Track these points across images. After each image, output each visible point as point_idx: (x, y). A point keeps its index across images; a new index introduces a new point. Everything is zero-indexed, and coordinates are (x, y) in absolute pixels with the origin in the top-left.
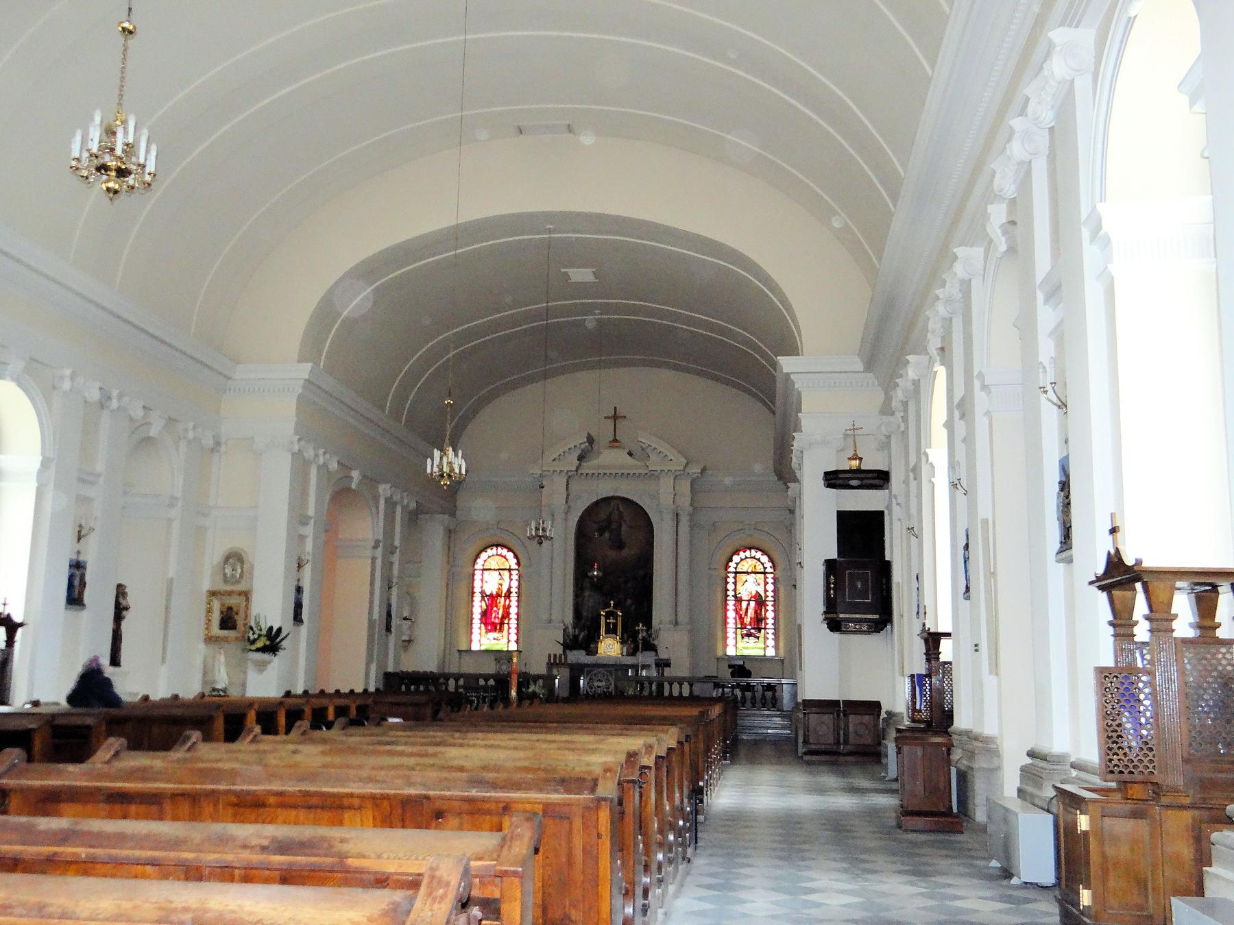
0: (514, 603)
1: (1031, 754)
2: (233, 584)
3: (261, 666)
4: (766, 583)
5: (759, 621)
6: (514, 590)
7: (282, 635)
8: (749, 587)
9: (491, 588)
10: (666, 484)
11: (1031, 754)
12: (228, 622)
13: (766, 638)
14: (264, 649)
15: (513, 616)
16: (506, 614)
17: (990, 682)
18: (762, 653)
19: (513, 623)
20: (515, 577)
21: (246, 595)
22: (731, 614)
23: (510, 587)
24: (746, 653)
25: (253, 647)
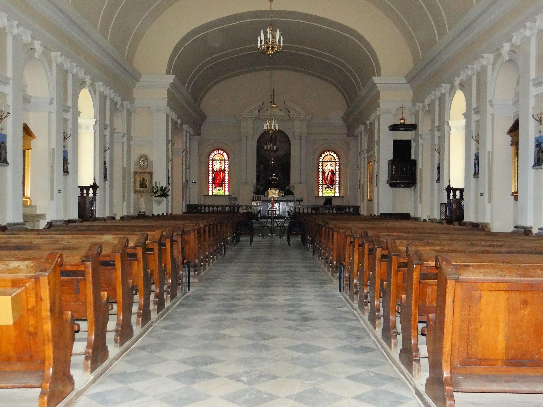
0: (227, 175)
1: (515, 227)
2: (144, 169)
3: (159, 203)
4: (336, 166)
5: (333, 181)
6: (227, 169)
7: (167, 190)
8: (329, 167)
9: (217, 167)
10: (297, 123)
11: (515, 227)
12: (143, 185)
13: (335, 189)
14: (161, 196)
15: (227, 180)
16: (224, 179)
17: (488, 206)
18: (333, 195)
19: (227, 182)
20: (227, 163)
21: (151, 174)
22: (321, 179)
23: (225, 168)
24: (327, 195)
25: (157, 195)
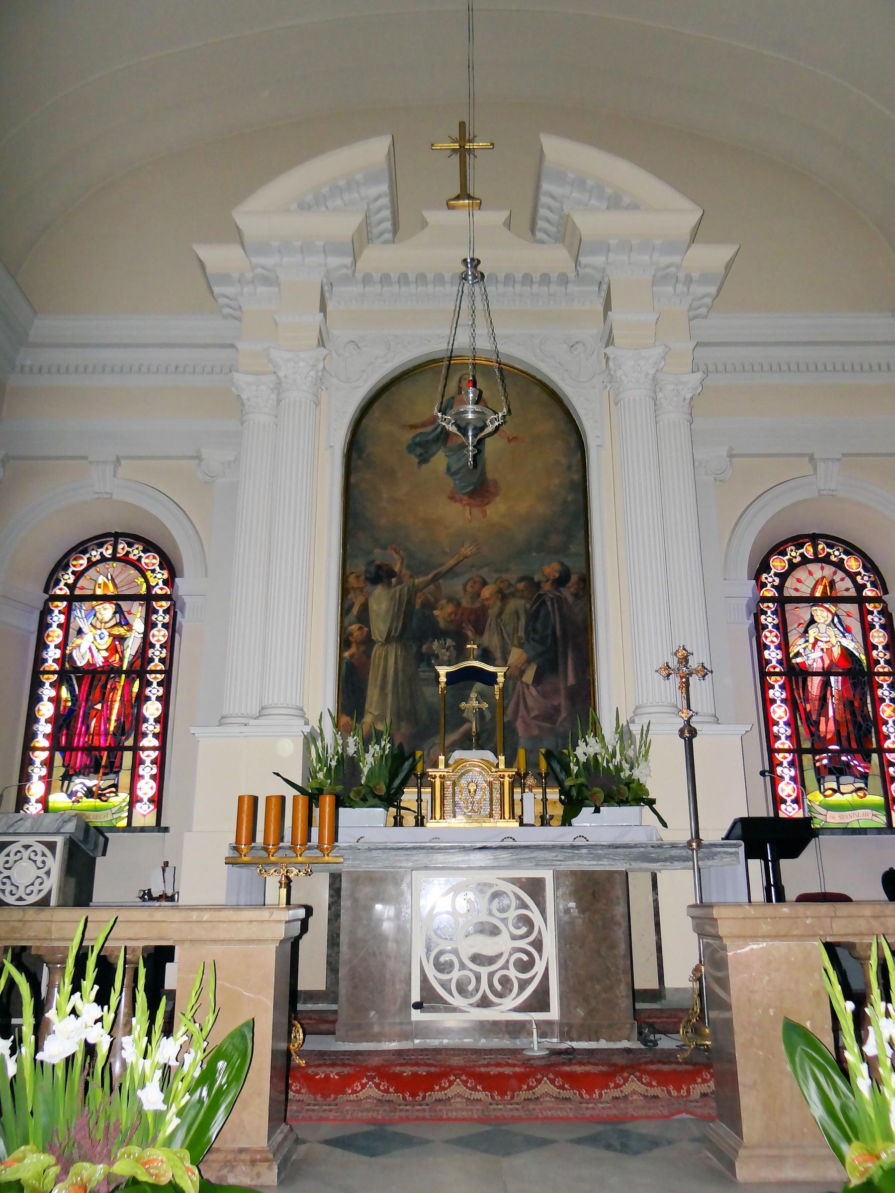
4: (867, 628)
9: (90, 648)
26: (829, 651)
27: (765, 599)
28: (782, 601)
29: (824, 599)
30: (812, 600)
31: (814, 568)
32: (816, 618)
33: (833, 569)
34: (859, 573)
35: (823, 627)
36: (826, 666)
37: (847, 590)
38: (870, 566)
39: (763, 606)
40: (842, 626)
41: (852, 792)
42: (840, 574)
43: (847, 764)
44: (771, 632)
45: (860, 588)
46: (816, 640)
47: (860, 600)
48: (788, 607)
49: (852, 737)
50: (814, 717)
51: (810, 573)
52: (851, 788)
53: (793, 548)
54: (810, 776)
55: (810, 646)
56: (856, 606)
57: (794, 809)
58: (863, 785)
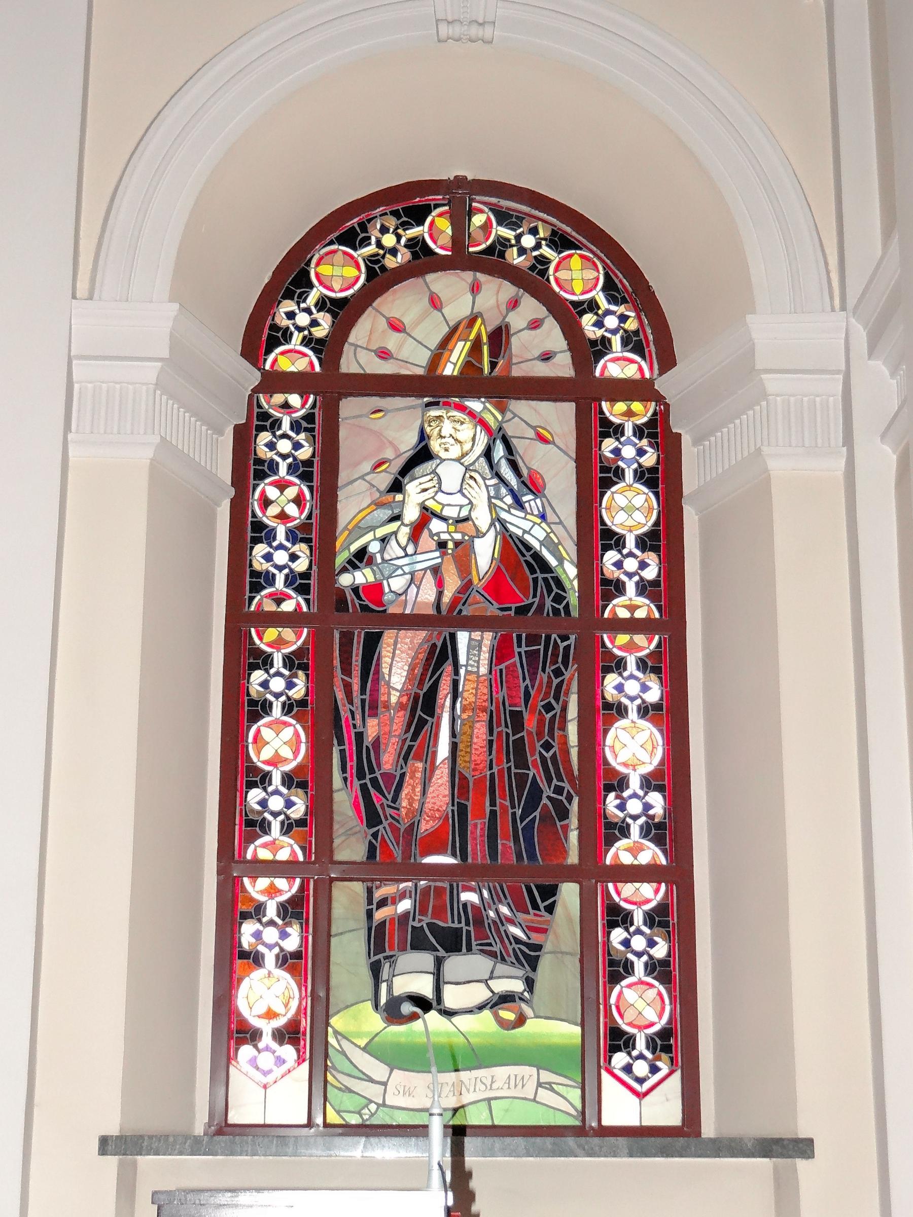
4: (595, 478)
26: (463, 553)
27: (274, 382)
28: (331, 387)
29: (471, 383)
30: (431, 388)
31: (451, 286)
32: (435, 446)
33: (508, 290)
34: (592, 306)
35: (451, 474)
36: (447, 598)
37: (546, 357)
38: (627, 281)
39: (272, 403)
40: (514, 465)
41: (481, 1008)
42: (531, 307)
43: (476, 915)
44: (282, 486)
45: (589, 351)
46: (427, 514)
47: (584, 392)
48: (349, 407)
49: (504, 825)
50: (388, 760)
51: (435, 303)
52: (480, 994)
53: (391, 222)
54: (349, 951)
55: (404, 534)
56: (569, 408)
57: (280, 1061)
58: (517, 986)
